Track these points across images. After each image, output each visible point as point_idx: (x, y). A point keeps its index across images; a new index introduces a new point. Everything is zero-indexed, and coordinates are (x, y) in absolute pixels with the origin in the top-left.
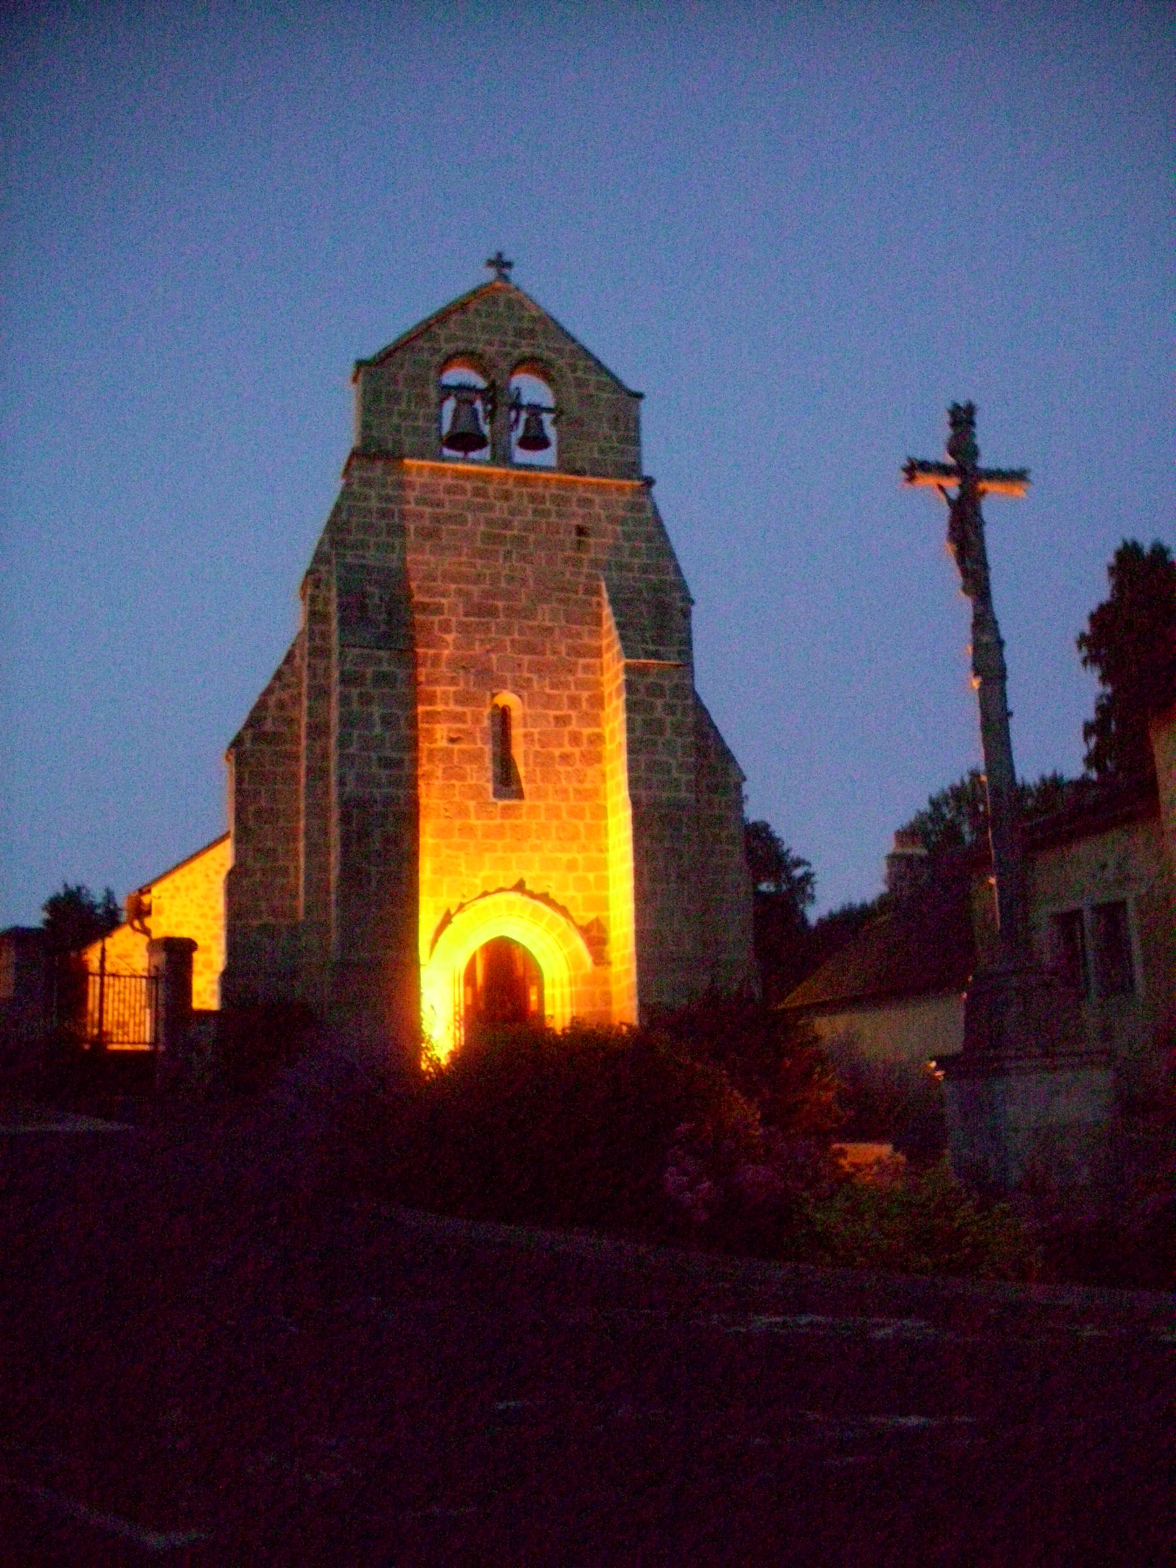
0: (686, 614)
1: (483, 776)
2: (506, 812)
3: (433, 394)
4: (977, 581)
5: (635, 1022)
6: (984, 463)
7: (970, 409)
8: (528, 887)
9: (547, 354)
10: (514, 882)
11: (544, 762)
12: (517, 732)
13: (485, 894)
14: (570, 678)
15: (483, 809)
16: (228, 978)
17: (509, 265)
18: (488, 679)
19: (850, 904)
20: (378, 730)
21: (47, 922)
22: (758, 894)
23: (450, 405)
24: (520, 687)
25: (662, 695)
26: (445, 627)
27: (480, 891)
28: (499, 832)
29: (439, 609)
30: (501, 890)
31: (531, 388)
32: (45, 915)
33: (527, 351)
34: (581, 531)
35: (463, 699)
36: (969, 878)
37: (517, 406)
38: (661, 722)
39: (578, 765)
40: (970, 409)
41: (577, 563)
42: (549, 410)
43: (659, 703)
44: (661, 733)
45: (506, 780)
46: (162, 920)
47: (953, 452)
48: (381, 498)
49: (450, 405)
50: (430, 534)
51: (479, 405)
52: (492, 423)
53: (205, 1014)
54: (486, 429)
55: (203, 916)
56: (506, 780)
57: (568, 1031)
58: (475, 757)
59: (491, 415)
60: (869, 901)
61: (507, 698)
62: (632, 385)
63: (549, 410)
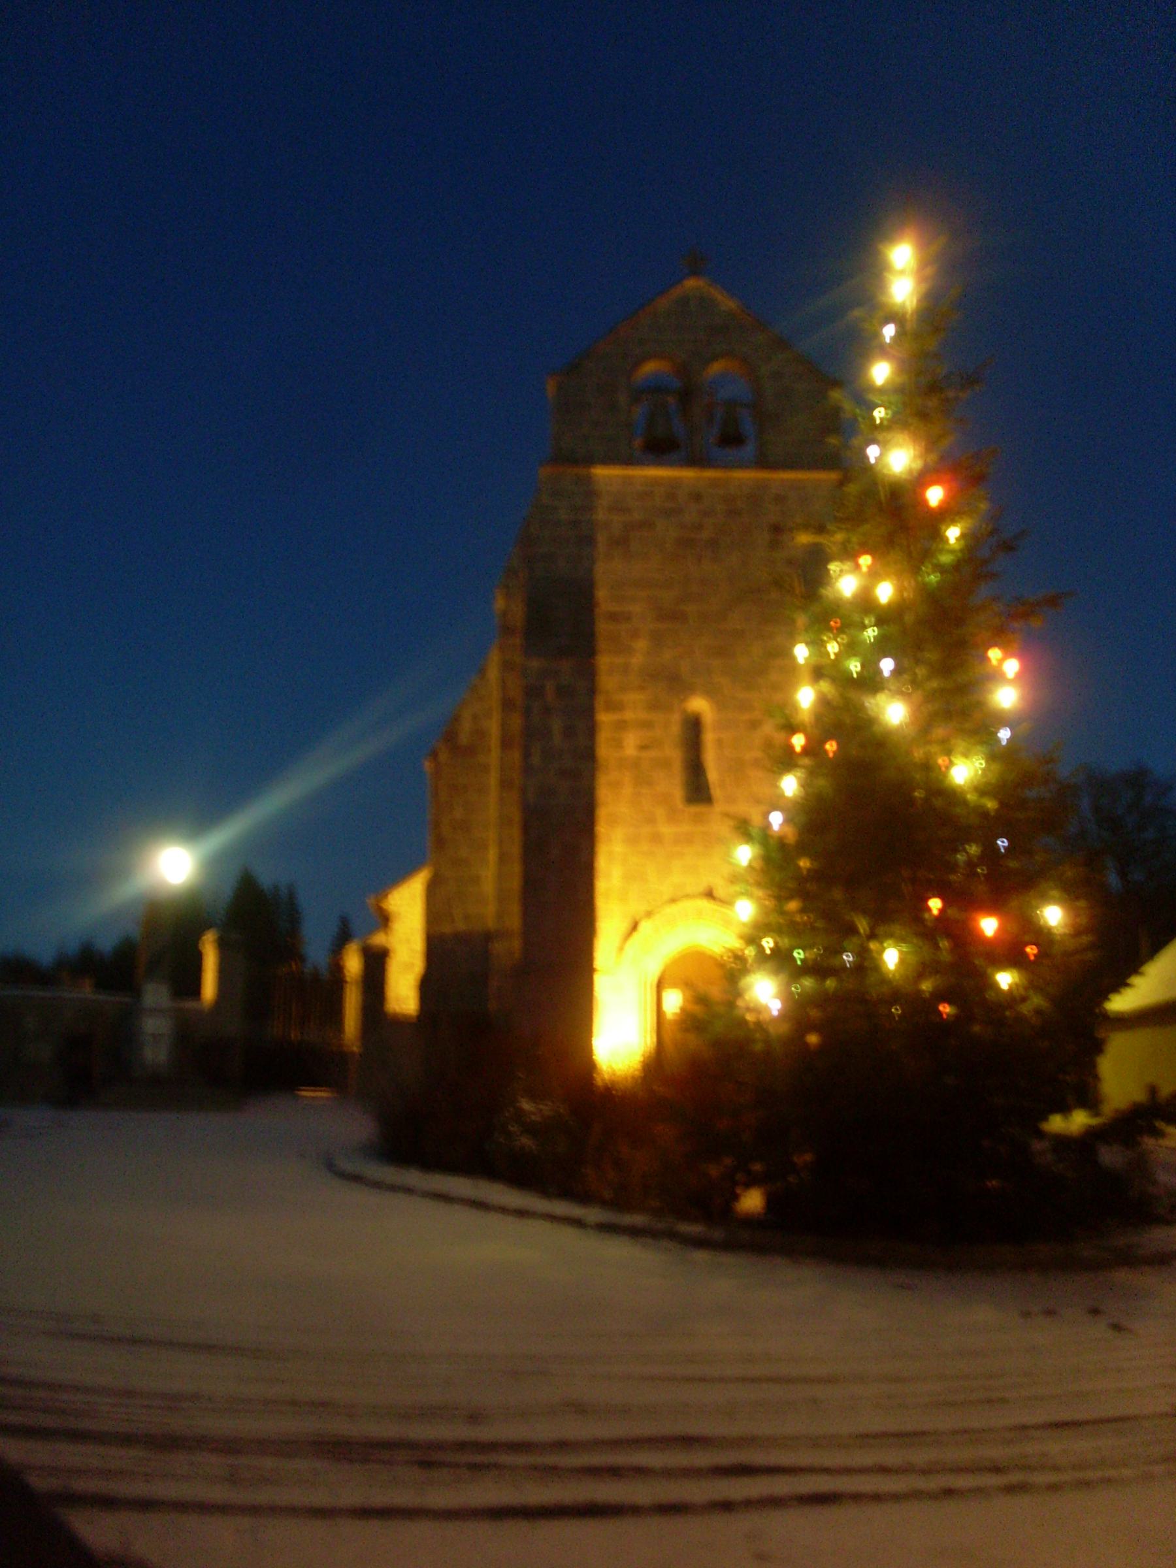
1: (673, 785)
2: (698, 819)
8: (717, 893)
10: (702, 888)
11: (737, 769)
12: (709, 738)
13: (673, 900)
15: (673, 816)
16: (427, 986)
18: (676, 683)
19: (1141, 974)
24: (711, 693)
26: (635, 635)
27: (666, 897)
28: (689, 840)
29: (627, 617)
30: (688, 896)
35: (654, 706)
36: (822, 641)
45: (698, 789)
50: (621, 542)
56: (698, 789)
57: (857, 313)
58: (665, 764)
61: (699, 704)
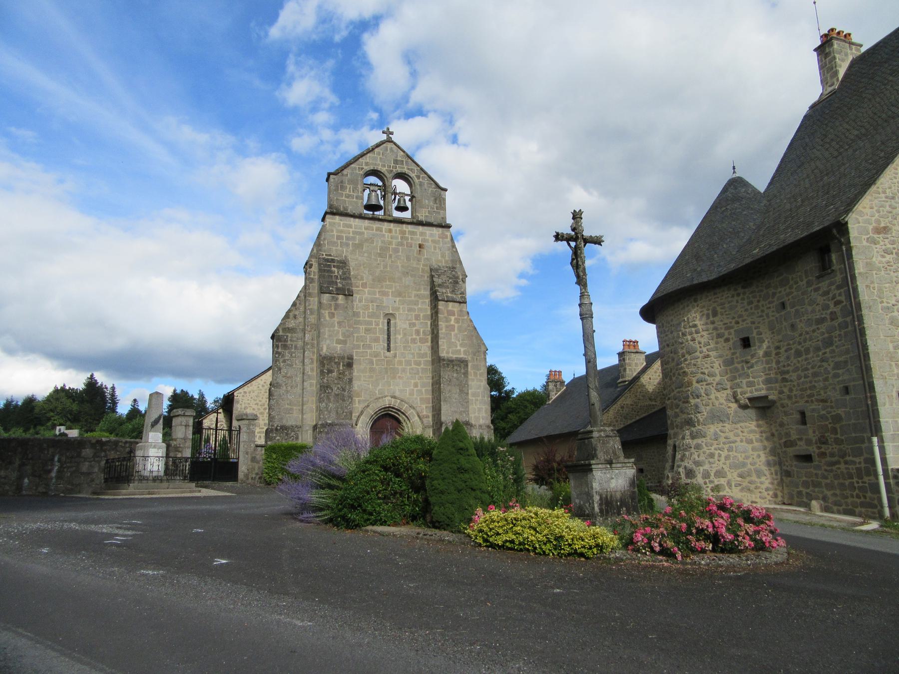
0: (464, 282)
3: (360, 188)
4: (581, 281)
5: (20, 403)
6: (587, 233)
7: (581, 212)
9: (407, 171)
14: (416, 307)
17: (392, 133)
20: (336, 328)
21: (84, 390)
22: (492, 396)
23: (367, 191)
25: (454, 315)
31: (401, 186)
32: (84, 387)
33: (399, 170)
34: (420, 246)
37: (395, 194)
38: (454, 326)
39: (419, 344)
40: (581, 212)
41: (419, 260)
42: (407, 195)
43: (453, 318)
44: (454, 330)
46: (239, 406)
47: (573, 230)
48: (338, 231)
49: (367, 191)
51: (379, 192)
52: (384, 200)
53: (80, 434)
54: (382, 203)
55: (257, 404)
59: (384, 197)
60: (366, 48)
62: (442, 185)
63: (407, 195)
